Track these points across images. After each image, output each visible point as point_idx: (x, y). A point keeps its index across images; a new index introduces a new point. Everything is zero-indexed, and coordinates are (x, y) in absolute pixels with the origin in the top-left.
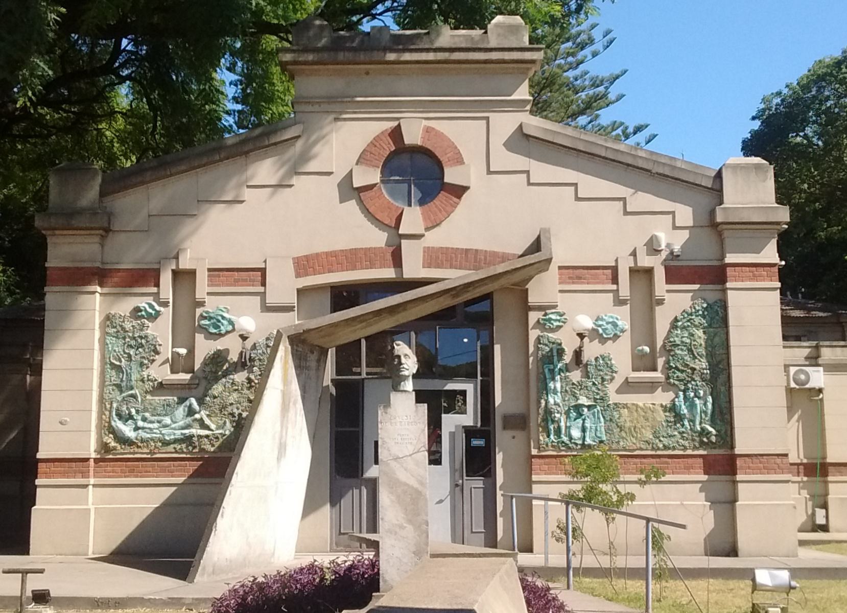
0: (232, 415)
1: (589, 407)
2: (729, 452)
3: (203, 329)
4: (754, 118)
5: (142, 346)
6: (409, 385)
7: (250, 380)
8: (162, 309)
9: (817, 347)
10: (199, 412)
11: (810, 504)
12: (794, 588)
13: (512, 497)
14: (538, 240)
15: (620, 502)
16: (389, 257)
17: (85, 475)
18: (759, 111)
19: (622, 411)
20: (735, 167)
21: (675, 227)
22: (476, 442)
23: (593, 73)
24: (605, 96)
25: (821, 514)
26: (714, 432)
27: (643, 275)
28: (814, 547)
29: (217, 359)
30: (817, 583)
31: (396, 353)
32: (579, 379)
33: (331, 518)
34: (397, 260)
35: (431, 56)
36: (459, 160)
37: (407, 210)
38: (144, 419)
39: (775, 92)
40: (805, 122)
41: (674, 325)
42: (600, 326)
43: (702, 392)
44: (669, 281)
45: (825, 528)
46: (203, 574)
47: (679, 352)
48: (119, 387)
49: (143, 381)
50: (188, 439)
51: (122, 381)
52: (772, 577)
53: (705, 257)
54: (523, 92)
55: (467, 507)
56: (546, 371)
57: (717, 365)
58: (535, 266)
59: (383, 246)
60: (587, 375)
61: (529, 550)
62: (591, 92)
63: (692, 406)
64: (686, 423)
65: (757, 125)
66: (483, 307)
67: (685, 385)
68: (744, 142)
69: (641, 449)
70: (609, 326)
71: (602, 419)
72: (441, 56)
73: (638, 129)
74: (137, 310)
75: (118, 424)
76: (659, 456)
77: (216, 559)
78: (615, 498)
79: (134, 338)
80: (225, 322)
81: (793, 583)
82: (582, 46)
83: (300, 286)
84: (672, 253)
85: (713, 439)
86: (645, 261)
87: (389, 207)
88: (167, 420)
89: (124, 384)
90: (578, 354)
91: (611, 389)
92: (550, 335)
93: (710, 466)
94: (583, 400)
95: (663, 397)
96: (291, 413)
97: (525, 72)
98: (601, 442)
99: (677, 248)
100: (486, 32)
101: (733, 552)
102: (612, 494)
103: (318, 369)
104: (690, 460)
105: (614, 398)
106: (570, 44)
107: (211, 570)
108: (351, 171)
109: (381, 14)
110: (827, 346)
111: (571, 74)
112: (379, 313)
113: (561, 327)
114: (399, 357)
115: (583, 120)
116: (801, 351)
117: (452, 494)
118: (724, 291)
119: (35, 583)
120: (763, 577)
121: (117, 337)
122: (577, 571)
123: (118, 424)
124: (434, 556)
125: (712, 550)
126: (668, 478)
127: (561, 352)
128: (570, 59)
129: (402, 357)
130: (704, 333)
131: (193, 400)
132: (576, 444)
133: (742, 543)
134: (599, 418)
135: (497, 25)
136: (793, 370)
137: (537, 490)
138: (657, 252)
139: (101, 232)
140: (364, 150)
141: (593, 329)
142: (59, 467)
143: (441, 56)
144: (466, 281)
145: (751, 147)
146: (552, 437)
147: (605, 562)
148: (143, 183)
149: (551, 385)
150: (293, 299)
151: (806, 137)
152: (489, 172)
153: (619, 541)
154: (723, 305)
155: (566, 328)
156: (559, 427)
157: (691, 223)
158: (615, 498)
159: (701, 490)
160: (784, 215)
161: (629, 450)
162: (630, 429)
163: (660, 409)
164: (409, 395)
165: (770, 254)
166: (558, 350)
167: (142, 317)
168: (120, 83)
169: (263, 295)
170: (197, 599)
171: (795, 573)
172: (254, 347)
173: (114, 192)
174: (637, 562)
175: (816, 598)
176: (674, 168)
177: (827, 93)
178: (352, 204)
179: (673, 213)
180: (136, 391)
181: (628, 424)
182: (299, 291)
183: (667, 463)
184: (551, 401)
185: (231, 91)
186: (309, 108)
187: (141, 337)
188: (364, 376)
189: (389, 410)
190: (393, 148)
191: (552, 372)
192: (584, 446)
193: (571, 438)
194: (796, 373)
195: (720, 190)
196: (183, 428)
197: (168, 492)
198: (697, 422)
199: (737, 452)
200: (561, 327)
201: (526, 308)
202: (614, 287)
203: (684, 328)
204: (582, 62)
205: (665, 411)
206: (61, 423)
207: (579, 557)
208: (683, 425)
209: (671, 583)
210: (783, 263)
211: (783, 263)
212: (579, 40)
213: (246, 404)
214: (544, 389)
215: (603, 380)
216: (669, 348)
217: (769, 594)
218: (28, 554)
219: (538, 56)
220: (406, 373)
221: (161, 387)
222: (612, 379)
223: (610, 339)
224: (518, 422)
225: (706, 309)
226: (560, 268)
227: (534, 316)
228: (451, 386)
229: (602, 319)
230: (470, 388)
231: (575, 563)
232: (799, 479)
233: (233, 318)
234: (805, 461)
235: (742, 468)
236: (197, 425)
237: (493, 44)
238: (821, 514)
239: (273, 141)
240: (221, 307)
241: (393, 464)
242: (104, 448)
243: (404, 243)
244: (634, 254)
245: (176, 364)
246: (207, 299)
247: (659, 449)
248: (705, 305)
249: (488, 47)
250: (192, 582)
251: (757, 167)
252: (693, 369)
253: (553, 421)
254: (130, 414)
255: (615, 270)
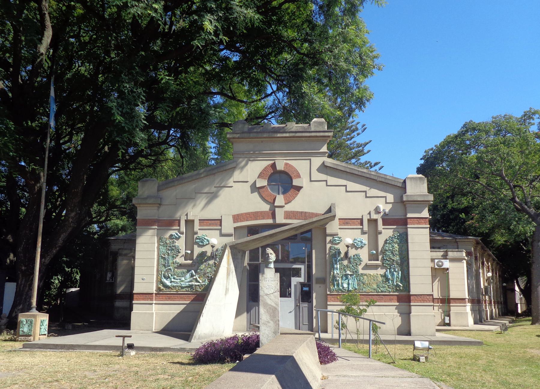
0: (208, 277)
1: (351, 275)
2: (408, 294)
3: (197, 243)
4: (421, 159)
5: (173, 250)
6: (272, 265)
7: (215, 263)
8: (181, 235)
9: (446, 252)
10: (195, 276)
11: (443, 315)
12: (431, 349)
13: (318, 311)
14: (330, 208)
15: (361, 313)
16: (270, 215)
17: (152, 300)
18: (424, 156)
19: (364, 277)
20: (411, 178)
21: (386, 203)
22: (305, 289)
23: (358, 142)
24: (362, 151)
25: (447, 319)
26: (402, 285)
27: (373, 222)
28: (444, 332)
29: (203, 254)
30: (443, 347)
31: (267, 252)
32: (347, 264)
33: (247, 318)
34: (274, 216)
35: (287, 135)
36: (299, 176)
37: (278, 196)
38: (174, 278)
39: (430, 148)
40: (442, 161)
41: (386, 242)
42: (355, 243)
43: (397, 270)
44: (384, 225)
45: (449, 325)
46: (194, 339)
47: (388, 253)
48: (164, 265)
49: (173, 263)
50: (191, 286)
51: (165, 263)
52: (422, 344)
53: (399, 215)
54: (324, 149)
55: (301, 314)
56: (334, 260)
57: (403, 259)
58: (329, 218)
59: (268, 210)
60: (350, 262)
61: (326, 332)
62: (357, 149)
63: (393, 275)
64: (390, 282)
65: (422, 162)
66: (308, 235)
67: (390, 266)
68: (417, 169)
69: (372, 292)
70: (359, 243)
71: (356, 280)
72: (291, 135)
73: (376, 164)
74: (171, 235)
75: (164, 280)
76: (379, 295)
77: (200, 333)
78: (359, 311)
79: (170, 247)
80: (205, 241)
81: (430, 347)
82: (353, 131)
83: (235, 226)
84: (385, 213)
85: (401, 288)
86: (374, 216)
87: (271, 195)
88: (183, 279)
89: (166, 264)
90: (346, 254)
91: (360, 268)
92: (335, 246)
93: (400, 299)
94: (348, 272)
95: (381, 271)
96: (231, 275)
97: (325, 141)
98: (356, 289)
99: (387, 211)
100: (310, 125)
101: (409, 334)
102: (357, 310)
103: (242, 259)
104: (392, 297)
105: (361, 271)
106: (348, 130)
107: (198, 338)
108: (256, 181)
109: (270, 119)
110: (451, 251)
111: (349, 142)
112: (266, 237)
113: (339, 243)
114: (268, 254)
115: (353, 161)
116: (439, 254)
117: (295, 309)
118: (407, 228)
119: (128, 341)
120: (418, 344)
121: (164, 246)
122: (343, 341)
123: (164, 280)
124: (281, 334)
125: (400, 333)
126: (377, 304)
127: (339, 253)
128: (348, 136)
129: (270, 255)
130: (398, 245)
131: (193, 271)
132: (345, 290)
133: (413, 330)
134: (355, 280)
135: (314, 122)
136: (436, 261)
137: (330, 308)
138: (380, 213)
139: (158, 205)
140: (261, 173)
141: (352, 244)
142: (142, 296)
143: (291, 135)
144: (301, 224)
145: (419, 171)
146: (336, 287)
147: (355, 337)
148: (174, 186)
149: (336, 266)
150: (232, 231)
151: (442, 166)
152: (311, 181)
153: (361, 329)
154: (406, 235)
155: (342, 243)
156: (339, 283)
157: (392, 201)
158: (359, 311)
159: (396, 309)
160: (431, 198)
161: (367, 293)
162: (367, 284)
163: (380, 276)
164: (272, 270)
165: (425, 213)
166: (338, 252)
167: (174, 238)
168: (171, 148)
169: (220, 230)
170: (191, 349)
171: (431, 342)
172: (217, 250)
173: (163, 190)
174: (367, 337)
175: (441, 353)
176: (386, 179)
177: (451, 149)
178: (256, 194)
179: (386, 197)
180: (171, 267)
181: (367, 282)
182: (235, 228)
183: (382, 298)
184: (335, 272)
185: (213, 150)
186: (239, 156)
187: (173, 246)
188: (260, 262)
189: (264, 275)
190: (272, 172)
191: (336, 261)
192: (349, 291)
193: (343, 288)
194: (437, 262)
195: (405, 188)
196: (189, 282)
197: (183, 307)
198: (395, 282)
199: (411, 294)
200: (339, 243)
201: (326, 235)
202: (361, 227)
203: (390, 243)
204: (353, 138)
205: (382, 277)
206: (142, 279)
207: (345, 335)
208: (389, 283)
209: (382, 346)
210: (431, 217)
211: (431, 217)
212: (352, 129)
213: (213, 273)
214: (333, 268)
215: (357, 264)
216: (384, 252)
217: (422, 351)
218: (130, 329)
219: (331, 134)
220: (271, 261)
221: (181, 266)
222: (360, 264)
223: (359, 248)
224: (322, 281)
225: (399, 236)
226: (339, 219)
227: (328, 239)
228: (295, 266)
229: (356, 240)
230: (302, 267)
231: (343, 337)
232: (438, 305)
233: (209, 239)
234: (441, 297)
235: (413, 300)
236: (194, 281)
237: (313, 129)
238: (447, 319)
239: (225, 168)
240: (204, 234)
241: (265, 297)
242: (159, 289)
243: (277, 209)
244: (370, 213)
245: (186, 257)
246: (199, 231)
247: (379, 292)
248: (398, 234)
249: (311, 131)
250: (190, 342)
251: (420, 178)
252: (393, 260)
253: (336, 281)
254: (169, 276)
255: (361, 220)
